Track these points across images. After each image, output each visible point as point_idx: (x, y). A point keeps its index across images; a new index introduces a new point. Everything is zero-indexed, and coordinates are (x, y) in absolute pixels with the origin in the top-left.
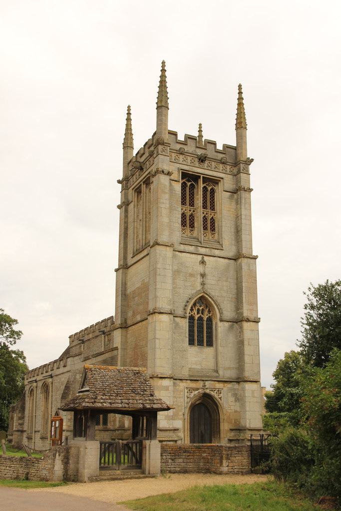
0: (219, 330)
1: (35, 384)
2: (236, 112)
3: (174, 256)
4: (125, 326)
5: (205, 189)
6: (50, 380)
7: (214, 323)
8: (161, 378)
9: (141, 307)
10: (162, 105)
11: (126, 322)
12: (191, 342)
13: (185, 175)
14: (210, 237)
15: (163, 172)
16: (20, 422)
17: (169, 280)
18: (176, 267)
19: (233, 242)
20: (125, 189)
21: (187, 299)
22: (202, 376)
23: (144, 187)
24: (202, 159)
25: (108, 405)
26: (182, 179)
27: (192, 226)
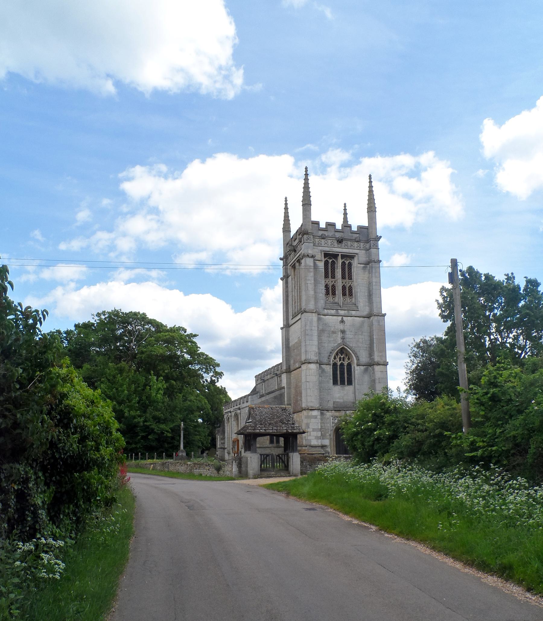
0: (356, 372)
1: (230, 414)
2: (367, 198)
3: (319, 319)
4: (289, 371)
5: (343, 264)
6: (239, 411)
7: (353, 367)
8: (311, 410)
9: (298, 358)
10: (307, 203)
11: (289, 368)
12: (335, 383)
13: (326, 255)
14: (349, 301)
15: (308, 256)
16: (222, 441)
17: (315, 338)
18: (321, 327)
19: (367, 304)
20: (285, 265)
21: (330, 351)
22: (344, 408)
23: (297, 264)
24: (340, 241)
25: (264, 431)
26: (325, 257)
27: (334, 294)
